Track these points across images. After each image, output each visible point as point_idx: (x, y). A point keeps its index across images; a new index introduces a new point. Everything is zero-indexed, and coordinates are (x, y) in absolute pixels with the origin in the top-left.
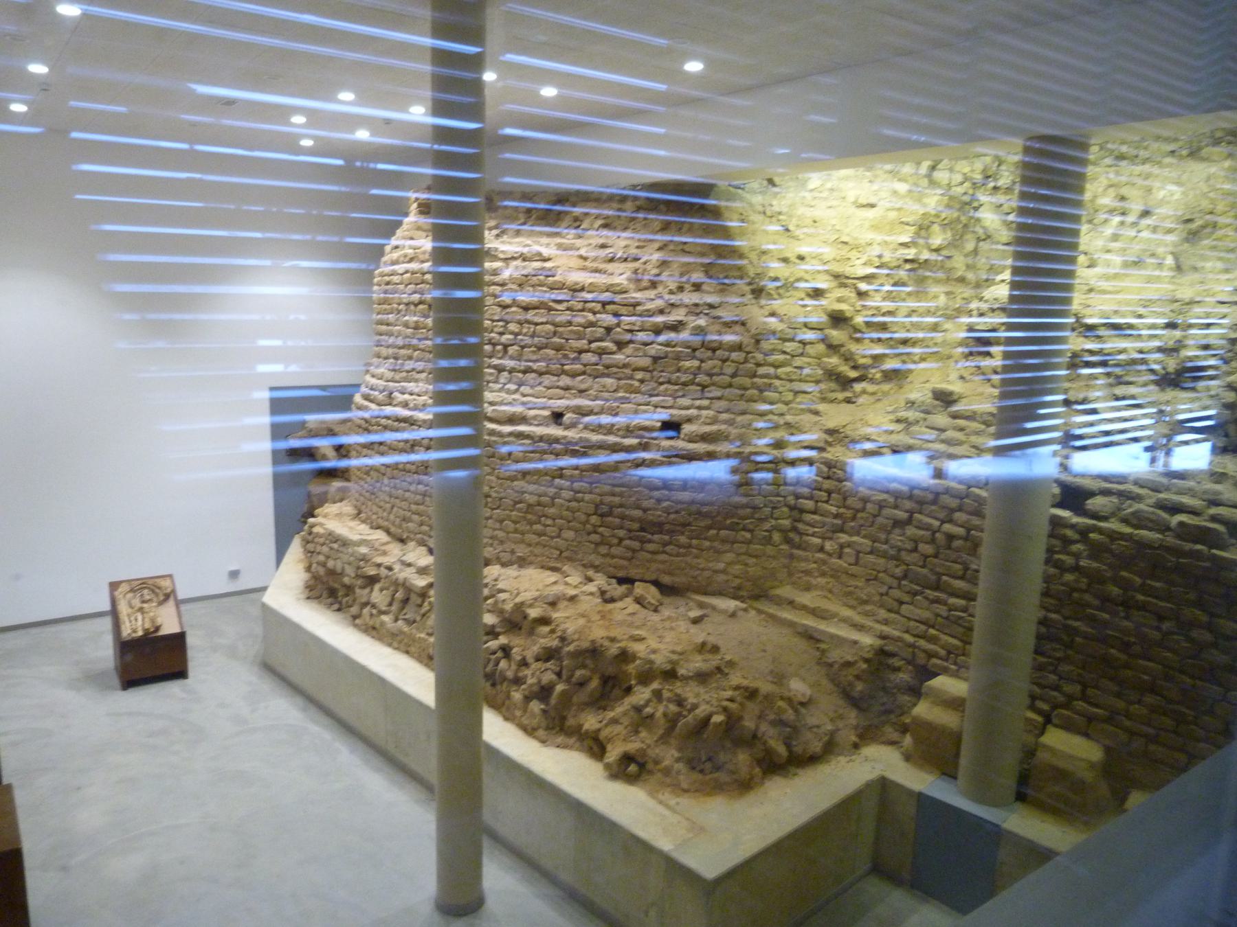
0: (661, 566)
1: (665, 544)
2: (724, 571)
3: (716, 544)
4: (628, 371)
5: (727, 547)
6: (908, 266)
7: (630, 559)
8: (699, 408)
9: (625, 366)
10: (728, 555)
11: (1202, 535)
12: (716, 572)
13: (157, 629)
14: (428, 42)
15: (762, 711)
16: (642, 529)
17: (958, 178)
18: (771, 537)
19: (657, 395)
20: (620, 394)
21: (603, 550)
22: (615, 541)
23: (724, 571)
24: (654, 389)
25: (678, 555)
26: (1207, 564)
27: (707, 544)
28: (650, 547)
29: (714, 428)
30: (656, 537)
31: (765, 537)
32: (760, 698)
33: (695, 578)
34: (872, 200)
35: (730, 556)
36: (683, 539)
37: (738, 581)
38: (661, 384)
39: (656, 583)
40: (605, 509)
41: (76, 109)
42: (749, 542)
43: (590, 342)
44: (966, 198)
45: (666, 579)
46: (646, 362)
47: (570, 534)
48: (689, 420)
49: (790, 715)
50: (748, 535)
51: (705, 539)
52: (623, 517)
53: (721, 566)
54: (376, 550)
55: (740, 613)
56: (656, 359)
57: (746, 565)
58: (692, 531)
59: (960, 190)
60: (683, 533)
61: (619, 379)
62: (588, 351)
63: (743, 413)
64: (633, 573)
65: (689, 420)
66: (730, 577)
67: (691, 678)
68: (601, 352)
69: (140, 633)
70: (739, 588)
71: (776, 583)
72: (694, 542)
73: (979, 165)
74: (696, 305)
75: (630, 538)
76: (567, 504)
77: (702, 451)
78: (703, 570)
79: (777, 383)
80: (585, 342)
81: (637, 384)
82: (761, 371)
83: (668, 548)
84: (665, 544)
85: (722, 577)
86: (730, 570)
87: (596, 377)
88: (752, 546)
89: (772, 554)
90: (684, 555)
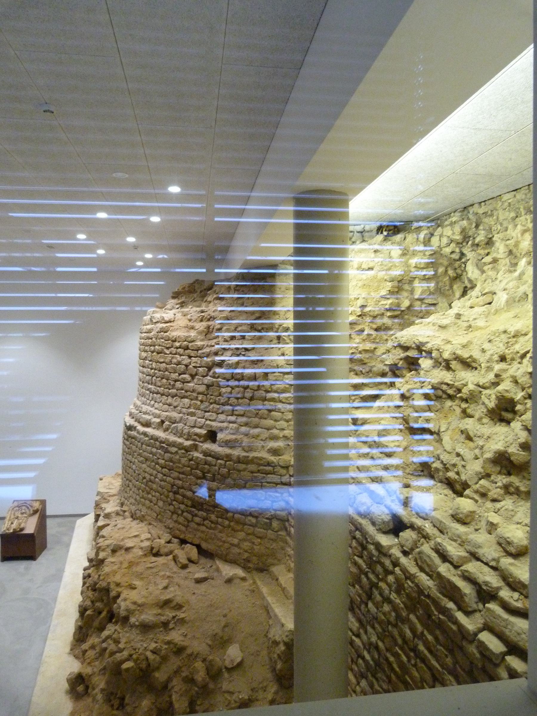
0: (202, 535)
1: (204, 519)
2: (237, 546)
3: (232, 524)
4: (195, 394)
5: (239, 527)
6: (389, 314)
7: (187, 527)
8: (230, 422)
9: (193, 391)
10: (240, 533)
11: (451, 591)
12: (233, 545)
13: (22, 529)
14: (292, 208)
15: (180, 667)
16: (193, 506)
17: (445, 241)
18: (271, 524)
19: (209, 412)
20: (191, 410)
21: (175, 517)
22: (180, 512)
23: (237, 546)
24: (206, 407)
25: (211, 528)
26: (454, 628)
27: (227, 522)
28: (197, 519)
29: (234, 437)
30: (201, 513)
31: (266, 523)
32: (184, 655)
33: (219, 547)
34: (371, 265)
35: (241, 535)
36: (213, 517)
37: (246, 555)
38: (211, 403)
39: (198, 547)
40: (175, 488)
41: (203, 268)
42: (254, 526)
43: (180, 375)
44: (456, 256)
45: (204, 545)
46: (202, 388)
47: (161, 503)
48: (221, 430)
49: (201, 676)
50: (254, 520)
51: (227, 519)
52: (184, 496)
53: (236, 541)
54: (105, 499)
55: (237, 581)
56: (208, 386)
57: (253, 543)
58: (218, 511)
59: (448, 250)
60: (213, 513)
61: (192, 400)
62: (178, 381)
63: (256, 427)
64: (188, 537)
65: (221, 430)
66: (241, 551)
67: (137, 627)
68: (184, 382)
69: (11, 531)
70: (248, 560)
71: (276, 561)
72: (220, 520)
73: (457, 229)
74: (237, 349)
75: (187, 511)
76: (160, 482)
77: (223, 453)
78: (224, 542)
79: (280, 406)
80: (177, 374)
81: (199, 403)
82: (269, 395)
83: (206, 522)
84: (204, 519)
85: (236, 550)
86: (241, 545)
87: (182, 398)
88: (256, 529)
89: (273, 537)
90: (214, 529)
